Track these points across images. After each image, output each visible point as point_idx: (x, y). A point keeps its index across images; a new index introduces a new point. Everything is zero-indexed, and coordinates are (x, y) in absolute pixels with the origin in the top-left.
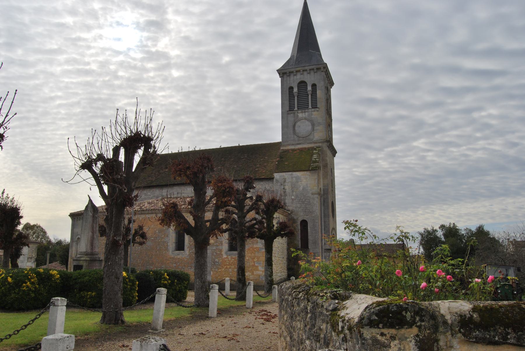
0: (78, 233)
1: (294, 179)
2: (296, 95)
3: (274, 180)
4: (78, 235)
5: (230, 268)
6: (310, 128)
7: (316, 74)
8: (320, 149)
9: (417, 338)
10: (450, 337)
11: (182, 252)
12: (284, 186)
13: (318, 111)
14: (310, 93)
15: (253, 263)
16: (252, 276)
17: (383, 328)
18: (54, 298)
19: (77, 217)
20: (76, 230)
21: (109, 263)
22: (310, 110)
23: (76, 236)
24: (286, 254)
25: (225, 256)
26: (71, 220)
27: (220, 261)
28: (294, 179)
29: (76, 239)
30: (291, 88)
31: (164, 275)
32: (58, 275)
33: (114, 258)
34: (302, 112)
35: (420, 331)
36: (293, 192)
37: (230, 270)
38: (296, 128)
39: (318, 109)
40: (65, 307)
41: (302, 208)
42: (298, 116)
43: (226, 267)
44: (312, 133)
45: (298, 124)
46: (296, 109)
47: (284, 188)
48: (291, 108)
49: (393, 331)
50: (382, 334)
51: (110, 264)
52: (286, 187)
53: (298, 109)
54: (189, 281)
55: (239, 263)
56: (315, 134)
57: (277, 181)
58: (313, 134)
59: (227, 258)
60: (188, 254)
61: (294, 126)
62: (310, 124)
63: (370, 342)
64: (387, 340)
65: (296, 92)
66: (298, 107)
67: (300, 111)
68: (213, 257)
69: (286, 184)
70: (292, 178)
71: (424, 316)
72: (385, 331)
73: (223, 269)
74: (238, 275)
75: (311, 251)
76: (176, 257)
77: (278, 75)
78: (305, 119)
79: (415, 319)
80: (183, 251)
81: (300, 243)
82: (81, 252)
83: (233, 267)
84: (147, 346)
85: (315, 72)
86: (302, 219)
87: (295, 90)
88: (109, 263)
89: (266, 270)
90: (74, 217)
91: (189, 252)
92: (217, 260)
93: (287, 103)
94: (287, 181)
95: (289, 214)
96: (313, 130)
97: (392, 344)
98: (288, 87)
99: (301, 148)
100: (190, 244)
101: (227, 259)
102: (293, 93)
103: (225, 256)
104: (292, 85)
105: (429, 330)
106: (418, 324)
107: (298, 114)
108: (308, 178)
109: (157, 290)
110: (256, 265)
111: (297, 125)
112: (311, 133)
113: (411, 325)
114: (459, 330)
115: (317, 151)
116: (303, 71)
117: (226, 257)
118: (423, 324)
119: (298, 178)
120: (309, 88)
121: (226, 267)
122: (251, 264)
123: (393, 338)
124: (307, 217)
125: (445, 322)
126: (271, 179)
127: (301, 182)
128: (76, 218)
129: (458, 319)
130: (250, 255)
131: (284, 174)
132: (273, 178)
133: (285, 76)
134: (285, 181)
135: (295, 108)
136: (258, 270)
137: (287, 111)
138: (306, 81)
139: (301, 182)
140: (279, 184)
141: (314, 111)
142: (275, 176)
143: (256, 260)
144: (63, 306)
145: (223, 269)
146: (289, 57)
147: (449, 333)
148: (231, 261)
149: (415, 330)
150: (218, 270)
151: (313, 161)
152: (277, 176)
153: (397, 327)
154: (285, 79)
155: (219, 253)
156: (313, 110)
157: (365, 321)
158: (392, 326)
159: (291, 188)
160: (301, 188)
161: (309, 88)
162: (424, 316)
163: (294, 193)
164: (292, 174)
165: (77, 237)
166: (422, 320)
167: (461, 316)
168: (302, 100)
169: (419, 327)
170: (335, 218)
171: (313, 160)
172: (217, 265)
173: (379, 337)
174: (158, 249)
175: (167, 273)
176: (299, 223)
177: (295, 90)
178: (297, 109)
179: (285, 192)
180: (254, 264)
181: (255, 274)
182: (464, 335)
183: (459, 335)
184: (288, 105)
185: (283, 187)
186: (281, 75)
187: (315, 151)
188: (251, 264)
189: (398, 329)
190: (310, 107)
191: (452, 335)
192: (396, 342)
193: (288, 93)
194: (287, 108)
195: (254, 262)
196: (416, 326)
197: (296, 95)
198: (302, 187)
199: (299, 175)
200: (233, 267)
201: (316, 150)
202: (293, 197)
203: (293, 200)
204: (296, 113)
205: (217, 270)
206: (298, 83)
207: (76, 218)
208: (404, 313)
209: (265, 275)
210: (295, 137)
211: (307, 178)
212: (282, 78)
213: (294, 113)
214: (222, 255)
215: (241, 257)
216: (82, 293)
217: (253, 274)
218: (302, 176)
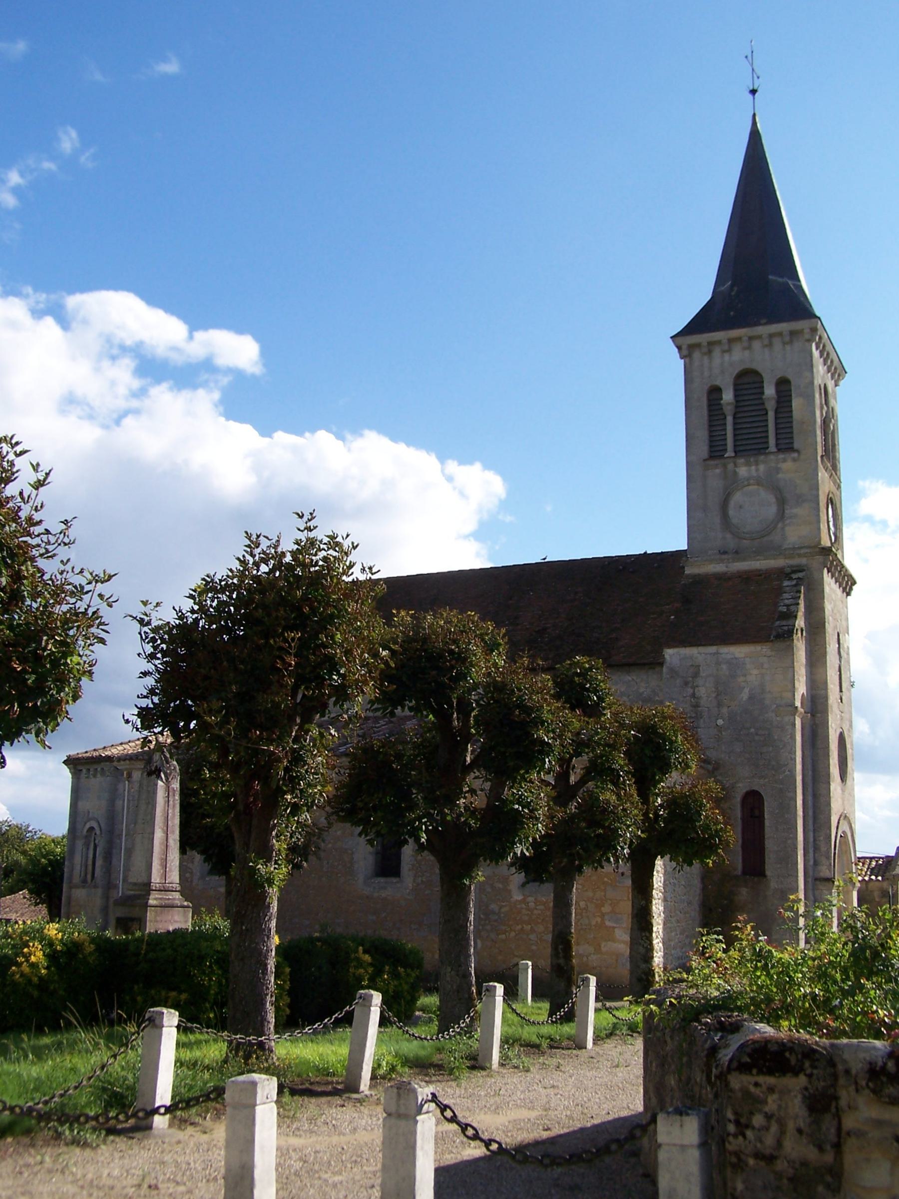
0: (91, 815)
1: (724, 667)
2: (729, 411)
3: (665, 669)
4: (89, 820)
5: (532, 931)
6: (772, 511)
7: (788, 347)
8: (800, 575)
9: (805, 1092)
10: (853, 1093)
11: (394, 880)
12: (694, 688)
13: (794, 460)
14: (771, 406)
15: (599, 920)
16: (594, 957)
17: (758, 1074)
18: (152, 1009)
19: (88, 767)
20: (82, 805)
21: (244, 928)
22: (772, 457)
23: (85, 823)
24: (698, 891)
25: (517, 896)
26: (70, 776)
27: (503, 910)
28: (724, 667)
29: (85, 830)
30: (715, 392)
31: (357, 951)
32: (92, 946)
33: (255, 915)
34: (748, 464)
35: (810, 1082)
36: (719, 705)
37: (532, 937)
38: (731, 513)
39: (795, 455)
40: (175, 1029)
41: (747, 755)
42: (735, 473)
43: (520, 927)
44: (780, 525)
45: (737, 497)
46: (730, 453)
47: (693, 695)
48: (715, 451)
49: (771, 1080)
50: (756, 1084)
51: (247, 930)
52: (702, 692)
53: (735, 452)
54: (420, 966)
55: (555, 925)
56: (787, 528)
57: (673, 672)
58: (783, 529)
59: (523, 901)
60: (411, 888)
61: (724, 506)
62: (772, 499)
63: (739, 1095)
64: (762, 1092)
65: (728, 404)
66: (735, 446)
67: (741, 461)
68: (484, 896)
69: (699, 681)
70: (718, 663)
71: (818, 1060)
72: (761, 1079)
73: (513, 934)
74: (555, 954)
75: (773, 884)
76: (376, 895)
77: (676, 350)
78: (759, 483)
79: (803, 1064)
80: (398, 879)
81: (740, 858)
82: (135, 884)
83: (541, 928)
84: (408, 1095)
85: (784, 343)
86: (748, 789)
87: (728, 396)
88: (244, 928)
89: (633, 943)
90: (80, 768)
91: (414, 881)
92: (493, 907)
93: (703, 434)
94: (702, 674)
95: (708, 771)
96: (781, 515)
97: (770, 1100)
98: (706, 388)
99: (746, 572)
100: (416, 860)
101: (524, 906)
102: (720, 404)
103: (517, 896)
104: (718, 383)
105: (824, 1081)
106: (808, 1071)
107: (737, 470)
108: (766, 666)
109: (358, 996)
110: (608, 923)
111: (732, 504)
112: (775, 527)
113: (796, 1071)
114: (867, 1085)
115: (794, 582)
116: (751, 338)
117: (520, 898)
118: (815, 1072)
119: (735, 666)
120: (770, 391)
121: (520, 927)
122: (594, 923)
123: (771, 1090)
124: (762, 781)
125: (847, 1072)
126: (657, 663)
127: (745, 675)
128: (84, 771)
129: (866, 1067)
130: (590, 894)
131: (693, 651)
132: (661, 664)
133: (697, 355)
134: (696, 675)
135: (726, 450)
136: (614, 940)
137: (705, 460)
138: (759, 369)
139: (745, 675)
140: (679, 681)
141: (784, 461)
142: (667, 657)
143: (606, 909)
144: (171, 1027)
145: (513, 934)
146: (708, 297)
147: (852, 1088)
148: (535, 912)
149: (802, 1079)
150: (498, 935)
151: (781, 612)
152: (670, 654)
153: (777, 1075)
154: (696, 363)
155: (501, 886)
156: (781, 456)
157: (735, 1064)
158: (770, 1072)
159: (714, 695)
160: (745, 695)
161: (770, 391)
162: (818, 1060)
163: (725, 710)
164: (717, 653)
165: (88, 826)
166: (813, 1067)
167: (870, 1063)
168: (754, 413)
169: (810, 1076)
170: (848, 782)
171: (780, 608)
172: (496, 921)
173: (752, 1089)
174: (325, 869)
175: (363, 945)
176: (738, 799)
177: (728, 396)
178: (733, 454)
179: (696, 706)
180: (603, 920)
181: (604, 949)
182: (874, 1091)
183: (867, 1091)
184: (707, 442)
185: (690, 691)
186: (685, 352)
187: (786, 583)
188: (594, 923)
189: (779, 1077)
190: (772, 447)
191: (857, 1091)
192: (775, 1096)
193: (705, 407)
194: (703, 450)
195: (603, 915)
196: (805, 1075)
197: (729, 411)
198: (746, 690)
199: (737, 655)
200: (541, 928)
201: (791, 579)
202: (720, 722)
203: (719, 728)
204: (730, 466)
205: (493, 936)
206: (734, 375)
207: (84, 771)
208: (787, 1054)
209: (631, 957)
210: (729, 536)
211: (762, 664)
212: (687, 360)
213: (725, 466)
214: (509, 891)
215: (562, 904)
216: (153, 992)
217: (598, 950)
218: (748, 660)
